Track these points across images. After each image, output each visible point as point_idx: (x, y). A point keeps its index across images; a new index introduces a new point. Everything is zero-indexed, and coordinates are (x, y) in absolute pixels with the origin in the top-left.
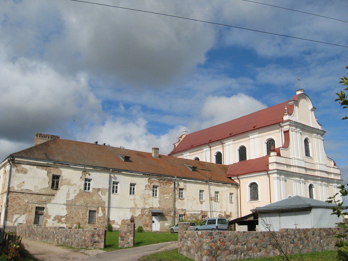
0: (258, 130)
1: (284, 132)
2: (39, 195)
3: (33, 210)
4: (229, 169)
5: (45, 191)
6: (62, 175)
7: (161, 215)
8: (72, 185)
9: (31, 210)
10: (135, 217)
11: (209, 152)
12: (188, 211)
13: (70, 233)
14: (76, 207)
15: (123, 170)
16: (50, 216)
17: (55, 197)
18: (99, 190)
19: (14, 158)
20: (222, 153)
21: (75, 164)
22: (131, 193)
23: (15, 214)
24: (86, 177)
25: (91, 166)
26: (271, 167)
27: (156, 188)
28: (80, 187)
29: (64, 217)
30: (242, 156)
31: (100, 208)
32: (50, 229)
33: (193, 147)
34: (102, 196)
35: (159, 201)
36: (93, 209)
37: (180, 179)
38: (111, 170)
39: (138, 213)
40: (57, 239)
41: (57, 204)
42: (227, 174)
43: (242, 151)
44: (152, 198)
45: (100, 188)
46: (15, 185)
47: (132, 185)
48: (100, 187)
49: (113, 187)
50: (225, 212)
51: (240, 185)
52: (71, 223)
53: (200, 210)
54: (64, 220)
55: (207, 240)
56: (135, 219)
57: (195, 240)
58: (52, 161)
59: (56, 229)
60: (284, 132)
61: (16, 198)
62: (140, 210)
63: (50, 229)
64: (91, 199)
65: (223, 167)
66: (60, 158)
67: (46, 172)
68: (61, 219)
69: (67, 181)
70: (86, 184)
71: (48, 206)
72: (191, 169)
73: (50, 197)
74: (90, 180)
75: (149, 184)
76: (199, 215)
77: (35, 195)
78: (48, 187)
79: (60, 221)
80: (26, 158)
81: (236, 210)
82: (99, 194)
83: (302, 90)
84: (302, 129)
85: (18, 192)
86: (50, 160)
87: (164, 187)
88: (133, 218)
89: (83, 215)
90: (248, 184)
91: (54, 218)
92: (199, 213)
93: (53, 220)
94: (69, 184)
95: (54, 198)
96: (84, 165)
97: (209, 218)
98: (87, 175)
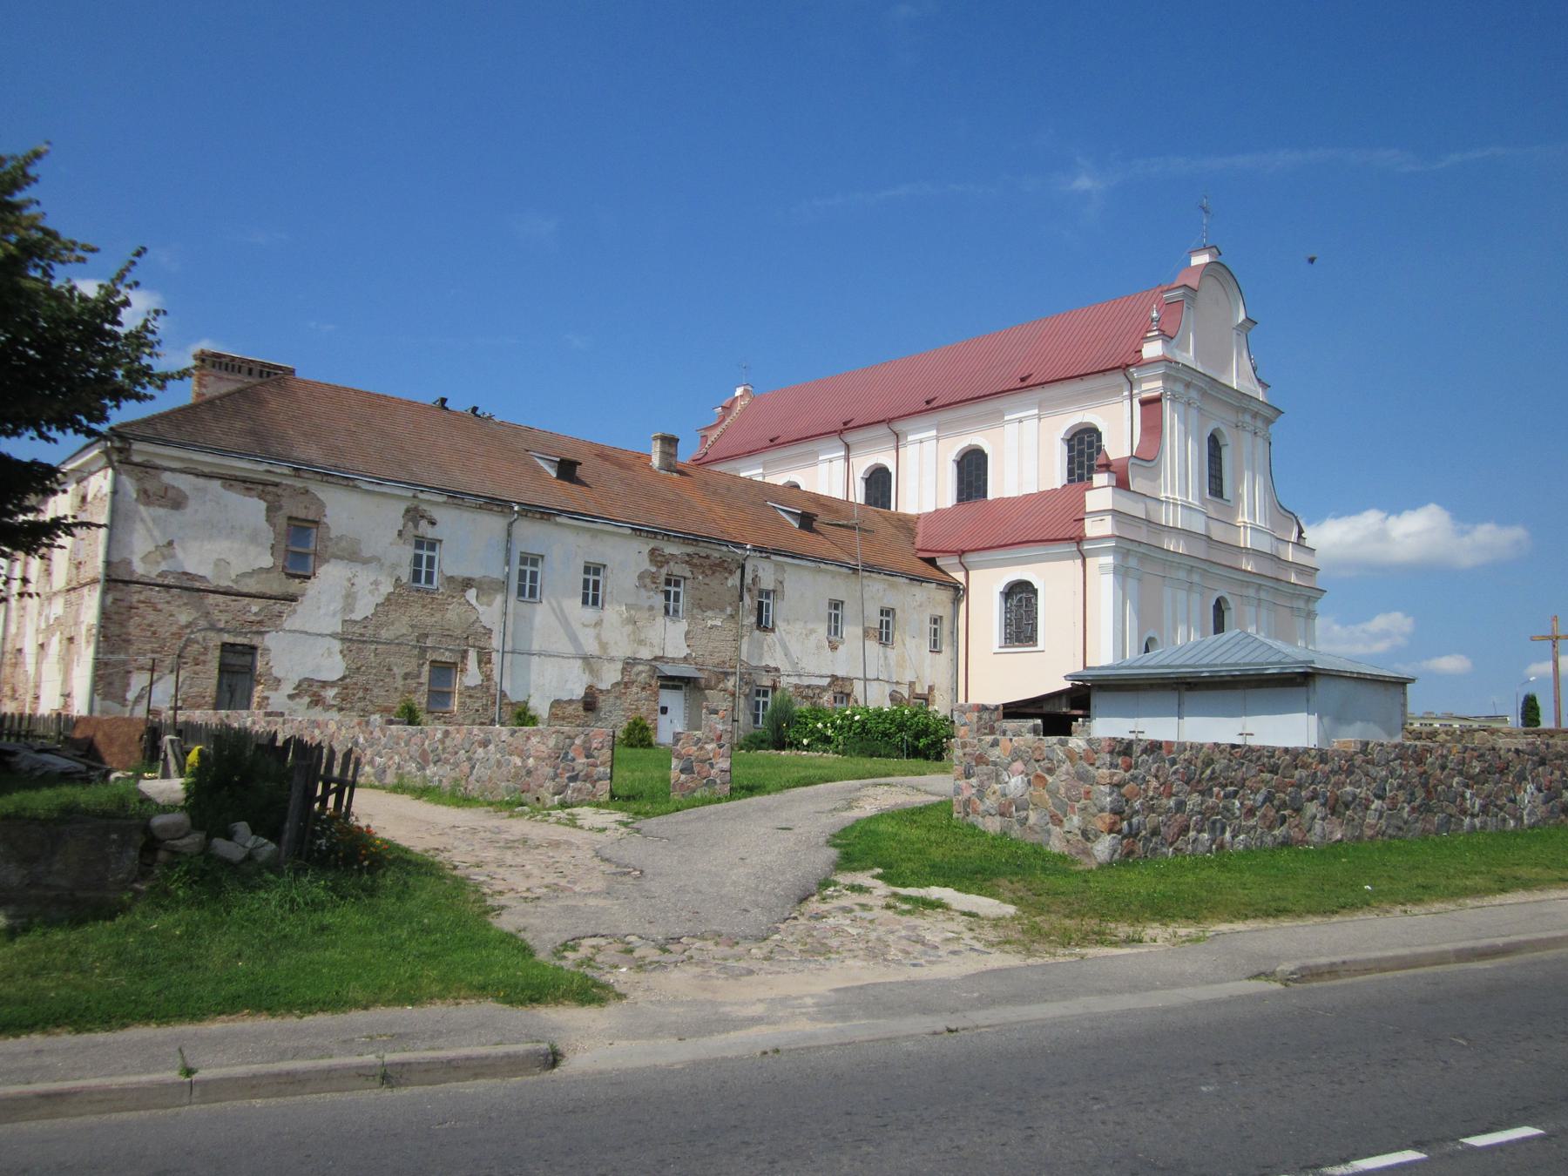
0: (1039, 394)
1: (1144, 403)
2: (234, 598)
3: (209, 657)
4: (920, 529)
5: (258, 583)
6: (325, 520)
7: (692, 685)
8: (366, 562)
9: (202, 658)
10: (601, 691)
11: (840, 465)
12: (788, 676)
13: (442, 741)
14: (379, 647)
15: (561, 512)
16: (280, 681)
17: (300, 609)
18: (467, 583)
19: (130, 444)
20: (892, 470)
21: (379, 479)
22: (585, 602)
23: (138, 669)
24: (420, 532)
25: (441, 491)
26: (1093, 528)
27: (677, 584)
28: (395, 569)
29: (333, 684)
30: (970, 484)
31: (472, 656)
32: (339, 729)
33: (776, 442)
34: (481, 609)
35: (687, 633)
36: (447, 657)
37: (764, 555)
38: (516, 508)
39: (610, 676)
40: (373, 767)
41: (306, 633)
42: (918, 545)
43: (972, 468)
44: (660, 620)
45: (473, 576)
46: (141, 558)
47: (593, 569)
48: (476, 573)
49: (522, 574)
50: (912, 684)
51: (966, 590)
52: (363, 710)
53: (830, 674)
54: (335, 697)
55: (1115, 774)
56: (601, 698)
57: (1050, 771)
58: (284, 461)
59: (371, 728)
60: (1144, 403)
61: (141, 605)
62: (620, 666)
63: (339, 729)
64: (438, 615)
65: (900, 520)
66: (311, 452)
67: (263, 505)
68: (322, 693)
69: (343, 544)
70: (417, 560)
71: (271, 641)
72: (795, 520)
73: (278, 607)
74: (433, 544)
75: (654, 569)
76: (824, 689)
77: (217, 596)
78: (271, 565)
79: (317, 701)
80: (180, 444)
81: (949, 676)
82: (467, 598)
83: (1215, 250)
84: (1203, 393)
85: (147, 581)
86: (280, 459)
87: (707, 581)
88: (593, 694)
89: (405, 679)
90: (1000, 586)
91: (294, 689)
92: (825, 682)
93: (291, 697)
94: (352, 555)
95: (295, 611)
96: (413, 485)
97: (856, 702)
98: (424, 523)
